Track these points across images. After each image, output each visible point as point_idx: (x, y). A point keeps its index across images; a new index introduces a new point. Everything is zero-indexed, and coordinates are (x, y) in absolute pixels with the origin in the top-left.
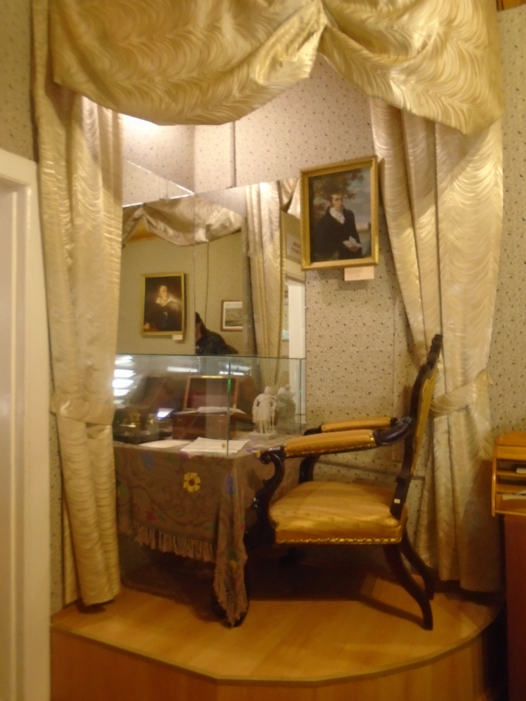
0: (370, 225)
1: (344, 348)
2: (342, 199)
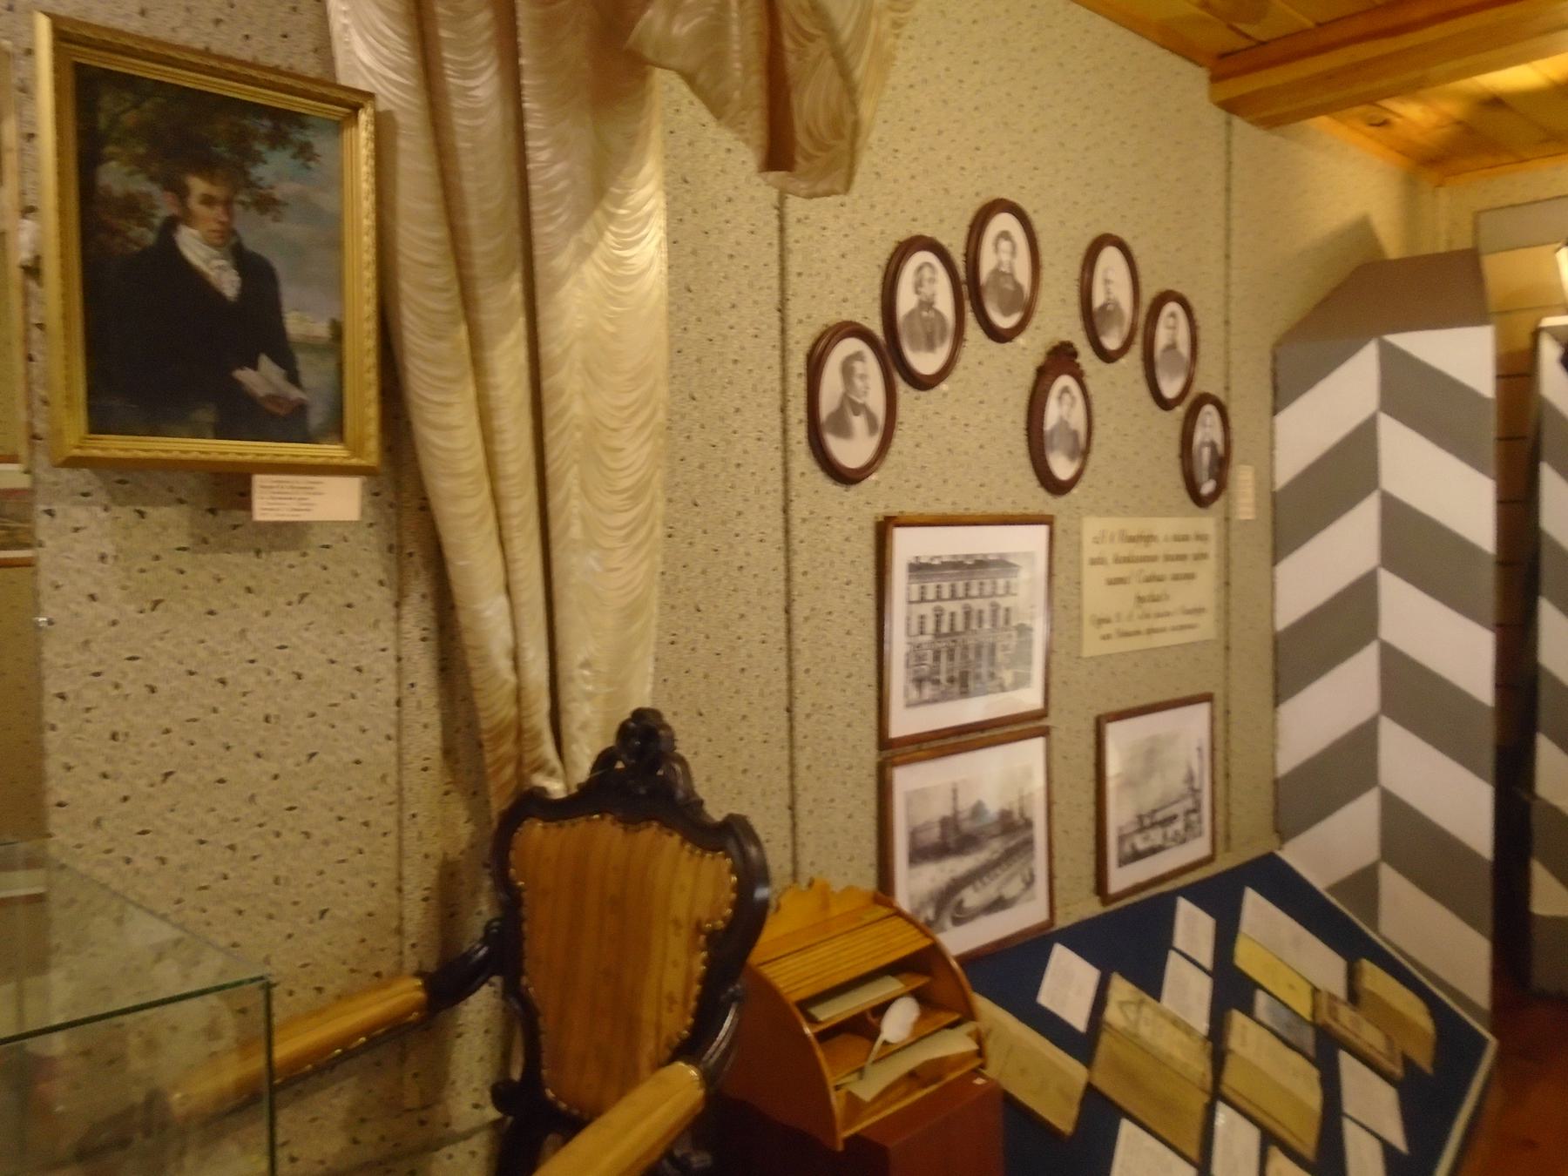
0: (337, 331)
1: (223, 772)
2: (228, 204)
